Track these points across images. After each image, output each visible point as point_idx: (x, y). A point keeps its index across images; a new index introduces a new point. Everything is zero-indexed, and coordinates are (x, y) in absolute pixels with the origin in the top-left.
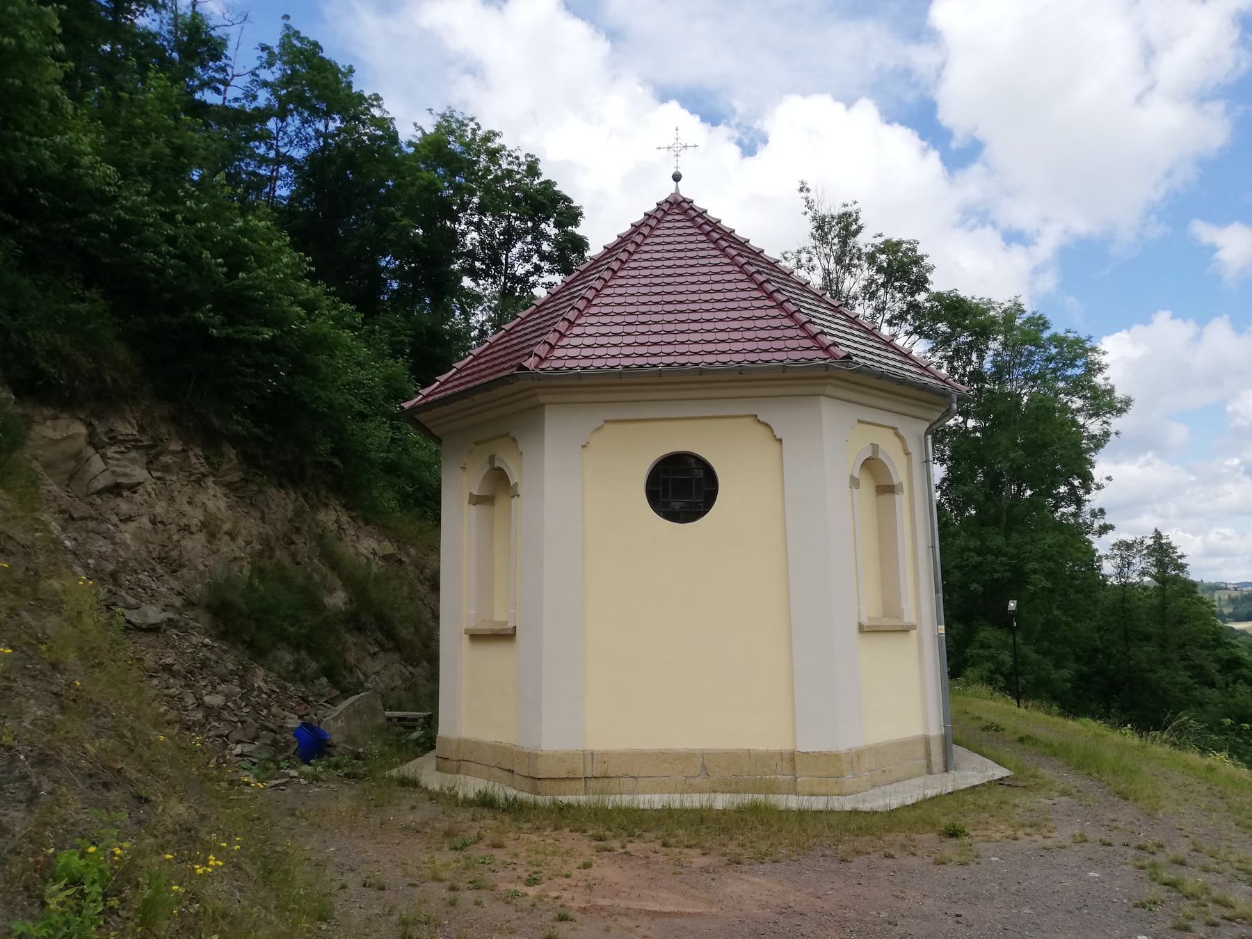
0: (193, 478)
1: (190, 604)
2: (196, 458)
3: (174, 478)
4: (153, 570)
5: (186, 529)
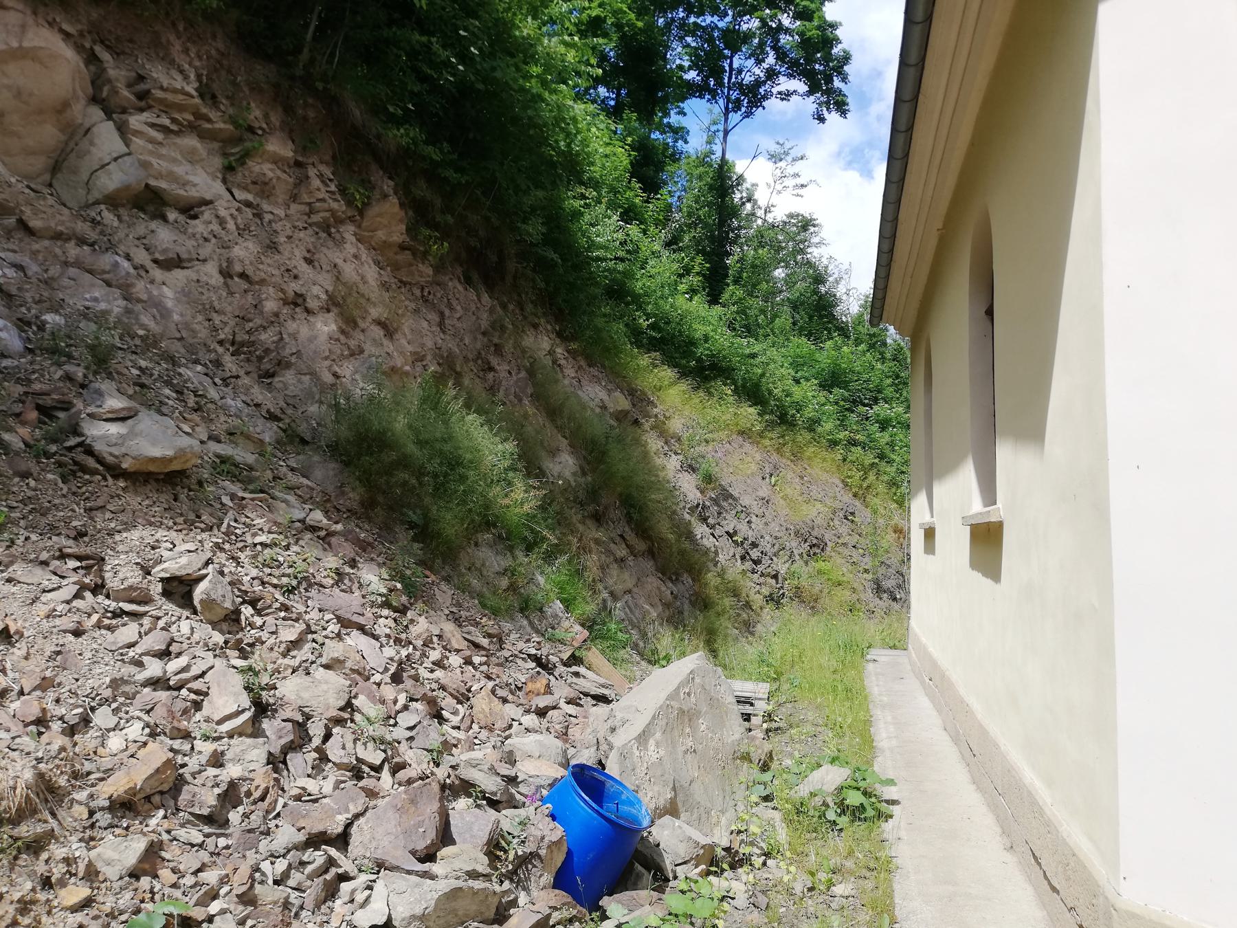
0: (315, 218)
2: (320, 183)
3: (280, 212)
4: (218, 363)
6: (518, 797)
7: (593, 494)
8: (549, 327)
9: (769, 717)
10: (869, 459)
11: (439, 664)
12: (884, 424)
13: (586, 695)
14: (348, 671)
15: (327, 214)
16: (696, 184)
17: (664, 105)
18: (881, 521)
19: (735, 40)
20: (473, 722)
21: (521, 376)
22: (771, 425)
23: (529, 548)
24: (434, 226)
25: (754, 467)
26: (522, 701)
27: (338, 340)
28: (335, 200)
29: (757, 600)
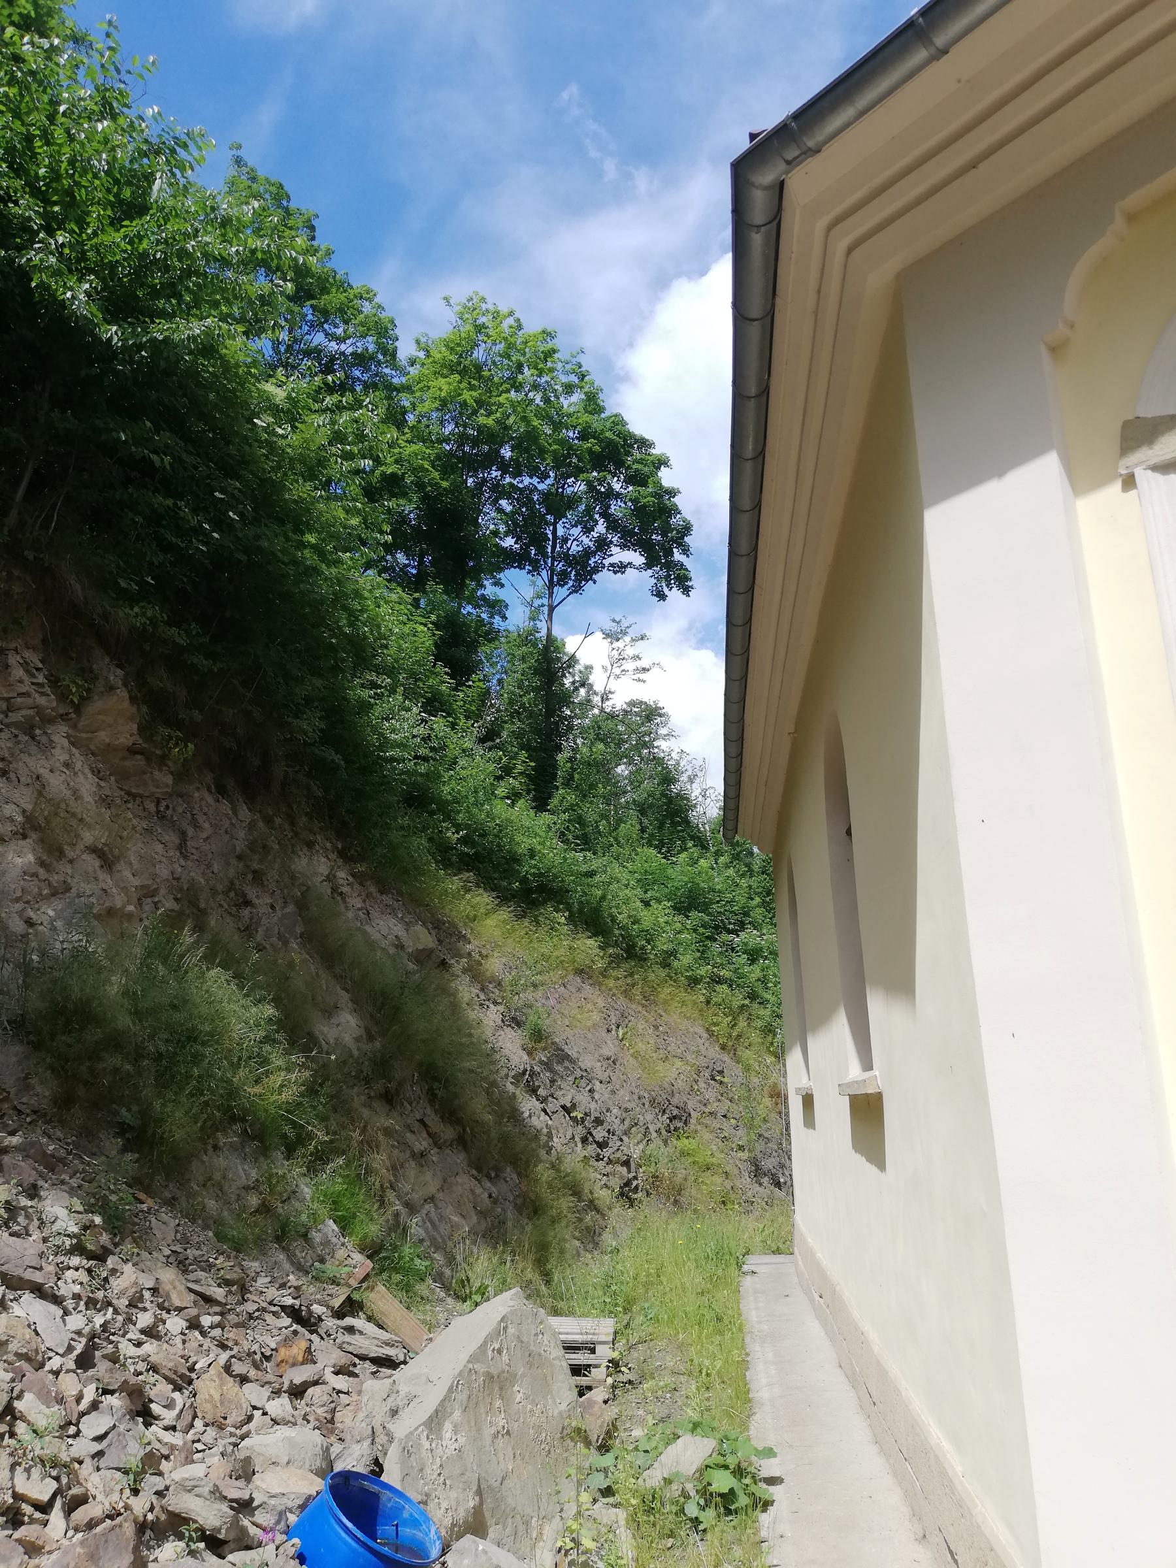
0: (14, 717)
6: (253, 1531)
7: (382, 1065)
8: (328, 845)
9: (615, 1364)
10: (738, 999)
11: (151, 1333)
12: (754, 955)
13: (363, 1358)
14: (11, 1357)
15: (31, 712)
16: (520, 666)
17: (476, 575)
18: (756, 1080)
19: (558, 504)
20: (195, 1416)
21: (287, 910)
22: (615, 961)
23: (290, 1152)
25: (596, 1017)
26: (270, 1377)
27: (35, 875)
28: (43, 694)
29: (603, 1196)
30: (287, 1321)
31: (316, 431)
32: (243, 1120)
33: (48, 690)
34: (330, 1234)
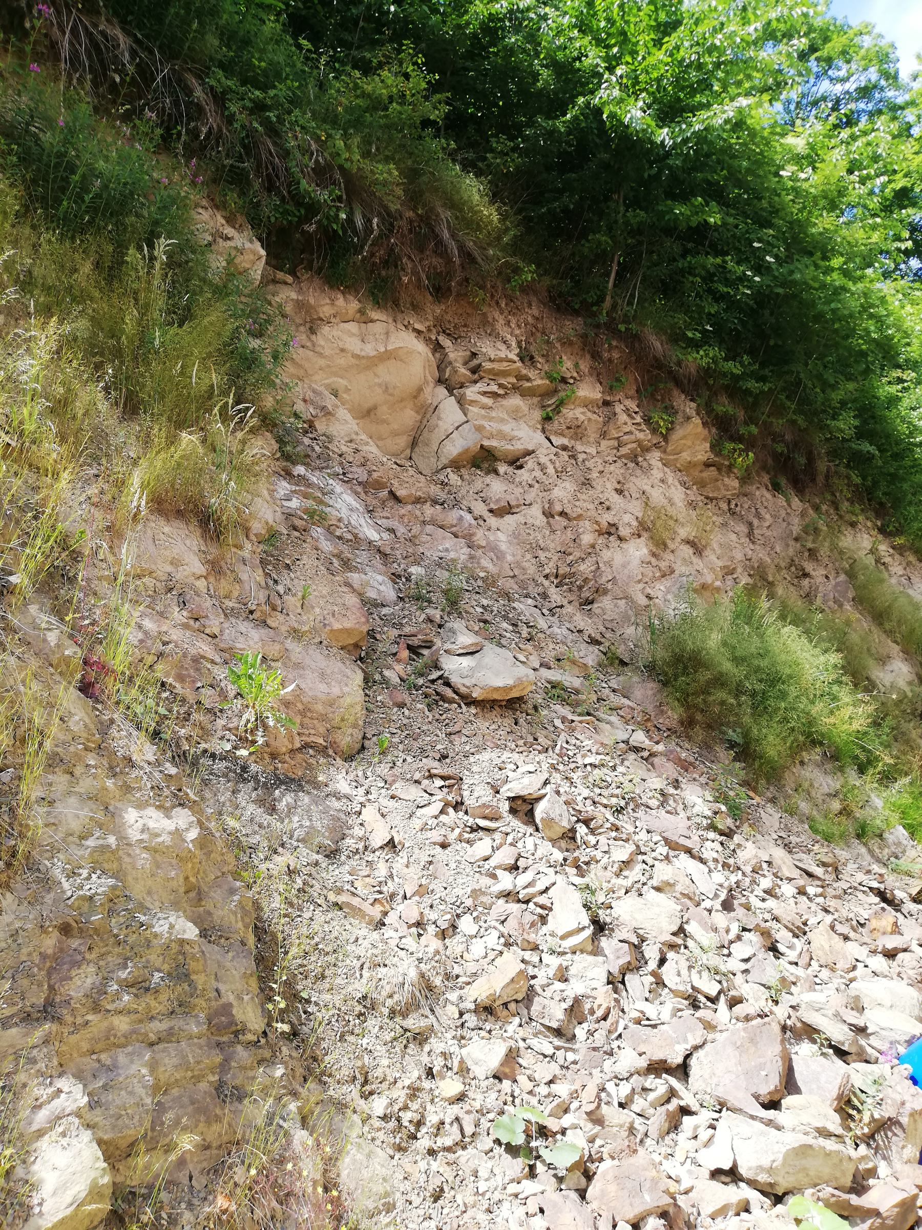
0: (624, 450)
1: (615, 662)
2: (627, 417)
3: (592, 450)
4: (545, 596)
5: (610, 531)
6: (869, 1050)
8: (869, 524)
15: (634, 445)
20: (811, 959)
23: (862, 770)
24: (740, 439)
27: (649, 563)
28: (641, 430)
30: (877, 900)
31: (835, 166)
32: (821, 744)
33: (644, 427)
34: (901, 837)
